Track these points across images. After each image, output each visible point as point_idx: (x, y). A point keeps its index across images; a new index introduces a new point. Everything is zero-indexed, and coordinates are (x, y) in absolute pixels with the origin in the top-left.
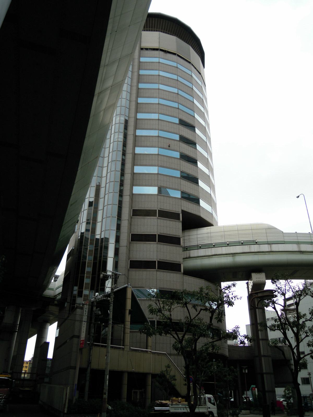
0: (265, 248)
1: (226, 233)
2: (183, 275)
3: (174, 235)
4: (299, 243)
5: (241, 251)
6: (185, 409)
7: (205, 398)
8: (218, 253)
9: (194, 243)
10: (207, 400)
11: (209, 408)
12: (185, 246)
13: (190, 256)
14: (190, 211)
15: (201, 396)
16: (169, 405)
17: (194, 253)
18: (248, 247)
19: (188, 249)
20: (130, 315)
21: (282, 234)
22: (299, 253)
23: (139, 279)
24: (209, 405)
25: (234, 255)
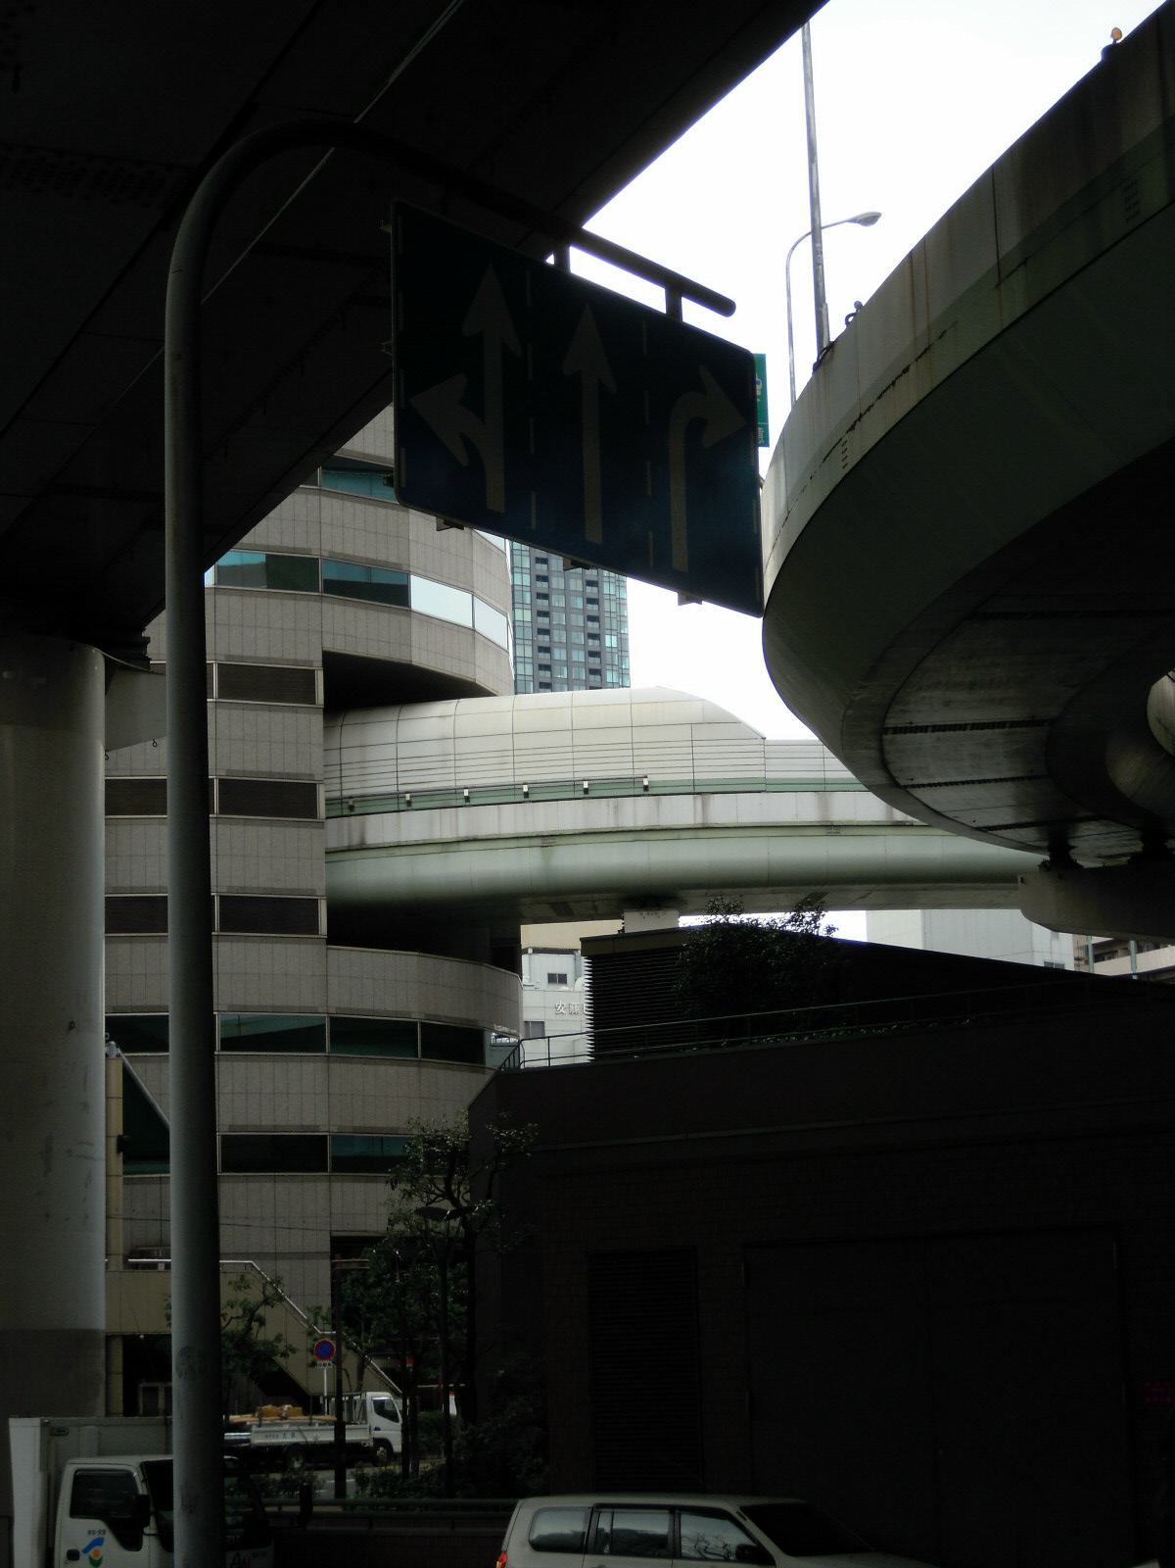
0: (681, 811)
1: (521, 742)
2: (324, 947)
3: (288, 774)
4: (828, 787)
5: (581, 826)
6: (296, 1434)
7: (364, 1403)
8: (482, 833)
9: (383, 784)
10: (370, 1407)
11: (377, 1429)
12: (345, 793)
13: (363, 842)
14: (361, 650)
15: (355, 1398)
16: (250, 1426)
17: (382, 828)
18: (611, 806)
19: (357, 811)
20: (121, 1154)
21: (761, 748)
22: (823, 831)
23: (146, 975)
24: (375, 1419)
25: (550, 840)
